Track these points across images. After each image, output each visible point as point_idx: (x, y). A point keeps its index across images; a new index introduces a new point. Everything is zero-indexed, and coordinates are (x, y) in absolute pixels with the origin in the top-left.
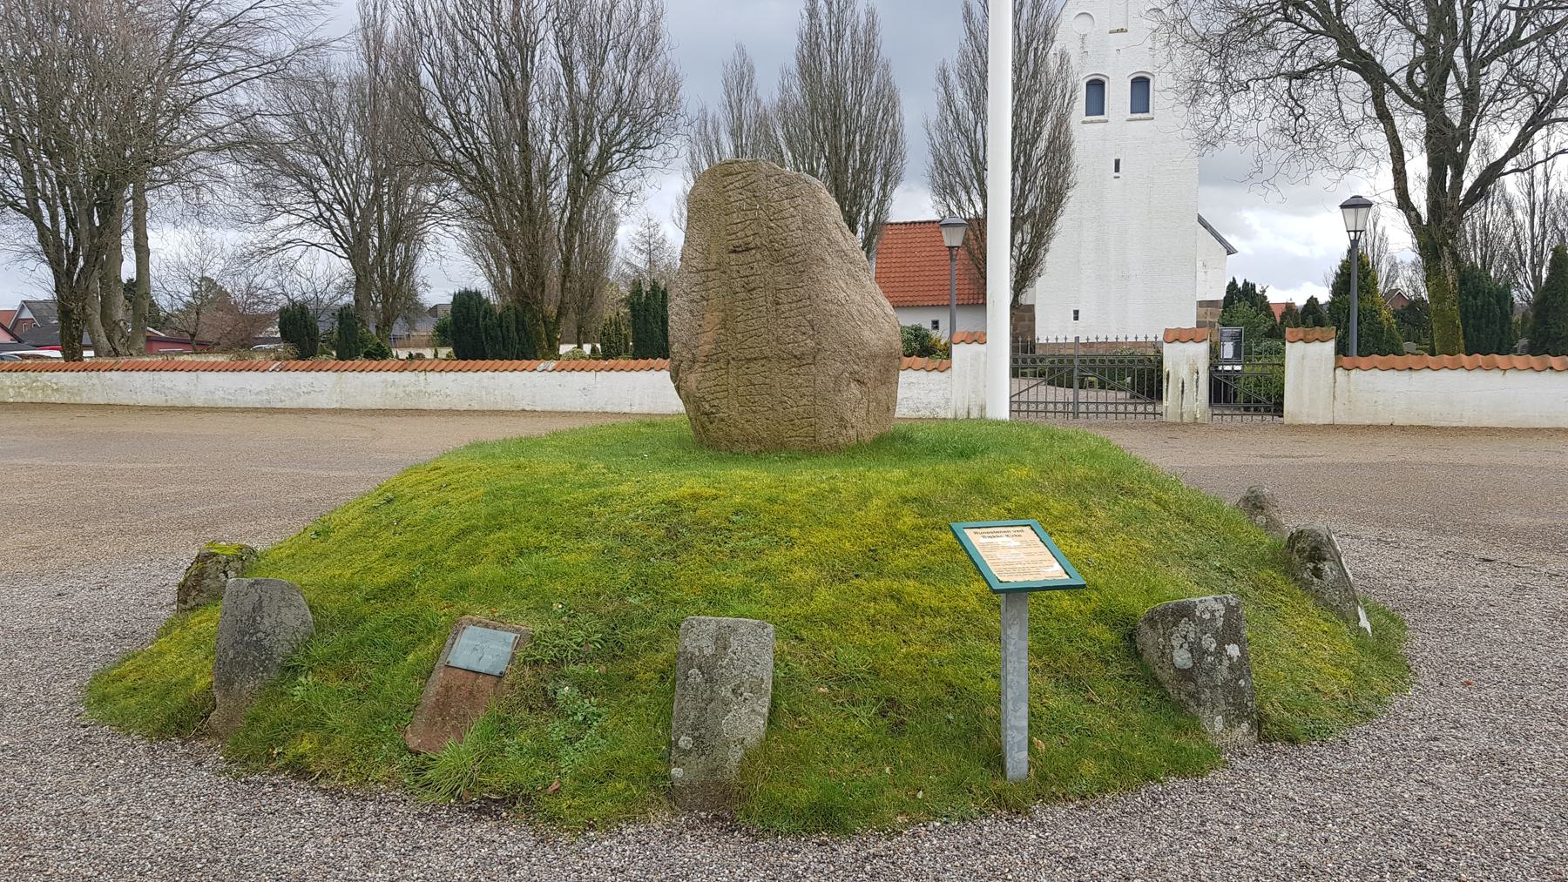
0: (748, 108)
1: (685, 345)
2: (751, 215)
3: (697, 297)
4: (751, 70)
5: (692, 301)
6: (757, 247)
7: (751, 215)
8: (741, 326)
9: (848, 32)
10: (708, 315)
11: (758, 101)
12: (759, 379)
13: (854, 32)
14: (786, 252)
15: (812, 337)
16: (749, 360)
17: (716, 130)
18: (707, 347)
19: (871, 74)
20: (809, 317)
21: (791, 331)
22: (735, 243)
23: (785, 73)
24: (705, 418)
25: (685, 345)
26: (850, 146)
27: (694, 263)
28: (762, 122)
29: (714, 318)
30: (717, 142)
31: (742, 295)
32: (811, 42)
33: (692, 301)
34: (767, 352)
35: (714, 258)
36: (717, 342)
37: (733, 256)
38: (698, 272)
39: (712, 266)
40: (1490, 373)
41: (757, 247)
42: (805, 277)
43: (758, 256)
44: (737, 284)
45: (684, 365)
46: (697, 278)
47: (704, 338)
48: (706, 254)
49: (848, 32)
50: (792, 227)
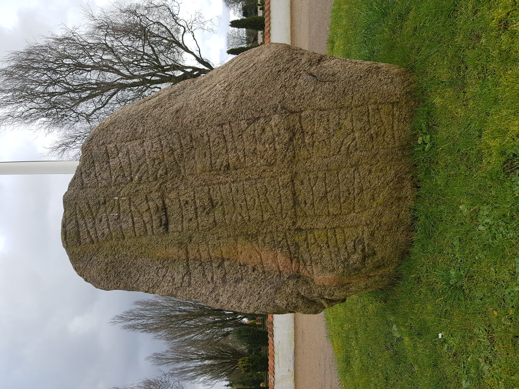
0: (169, 355)
1: (277, 289)
2: (124, 206)
3: (218, 274)
4: (155, 354)
5: (224, 281)
6: (163, 197)
7: (124, 206)
8: (253, 214)
9: (142, 312)
10: (242, 259)
11: (167, 351)
12: (319, 188)
13: (142, 310)
14: (168, 160)
15: (268, 119)
16: (296, 203)
17: (177, 369)
18: (281, 259)
19: (158, 302)
20: (243, 124)
21: (260, 147)
22: (155, 224)
23: (156, 338)
24: (369, 262)
25: (277, 289)
26: (184, 311)
27: (178, 278)
28: (175, 349)
29: (245, 251)
30: (181, 369)
31: (218, 214)
32: (146, 328)
33: (224, 281)
34: (286, 178)
35: (173, 251)
36: (275, 245)
37: (171, 227)
38: (188, 273)
39: (182, 253)
40: (271, 17)
41: (163, 197)
42: (196, 133)
43: (173, 195)
44: (205, 221)
45: (303, 290)
46: (196, 273)
47: (269, 264)
48: (167, 262)
49: (142, 312)
50: (140, 152)
